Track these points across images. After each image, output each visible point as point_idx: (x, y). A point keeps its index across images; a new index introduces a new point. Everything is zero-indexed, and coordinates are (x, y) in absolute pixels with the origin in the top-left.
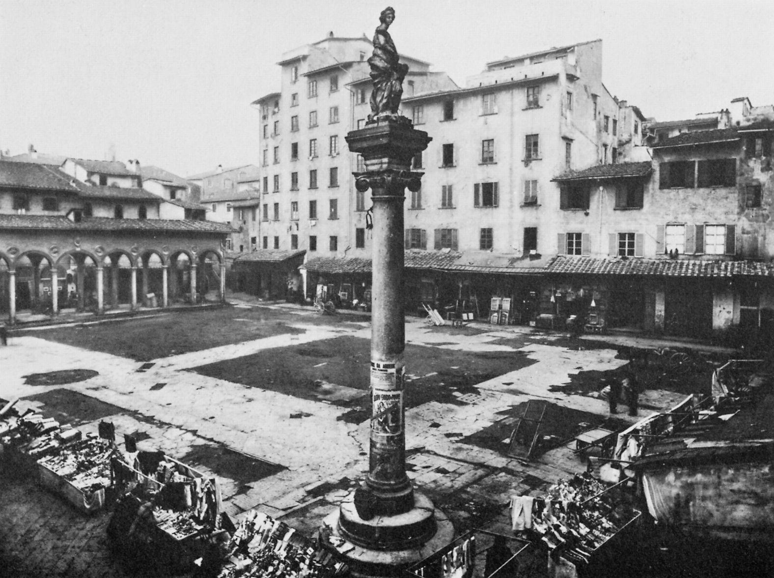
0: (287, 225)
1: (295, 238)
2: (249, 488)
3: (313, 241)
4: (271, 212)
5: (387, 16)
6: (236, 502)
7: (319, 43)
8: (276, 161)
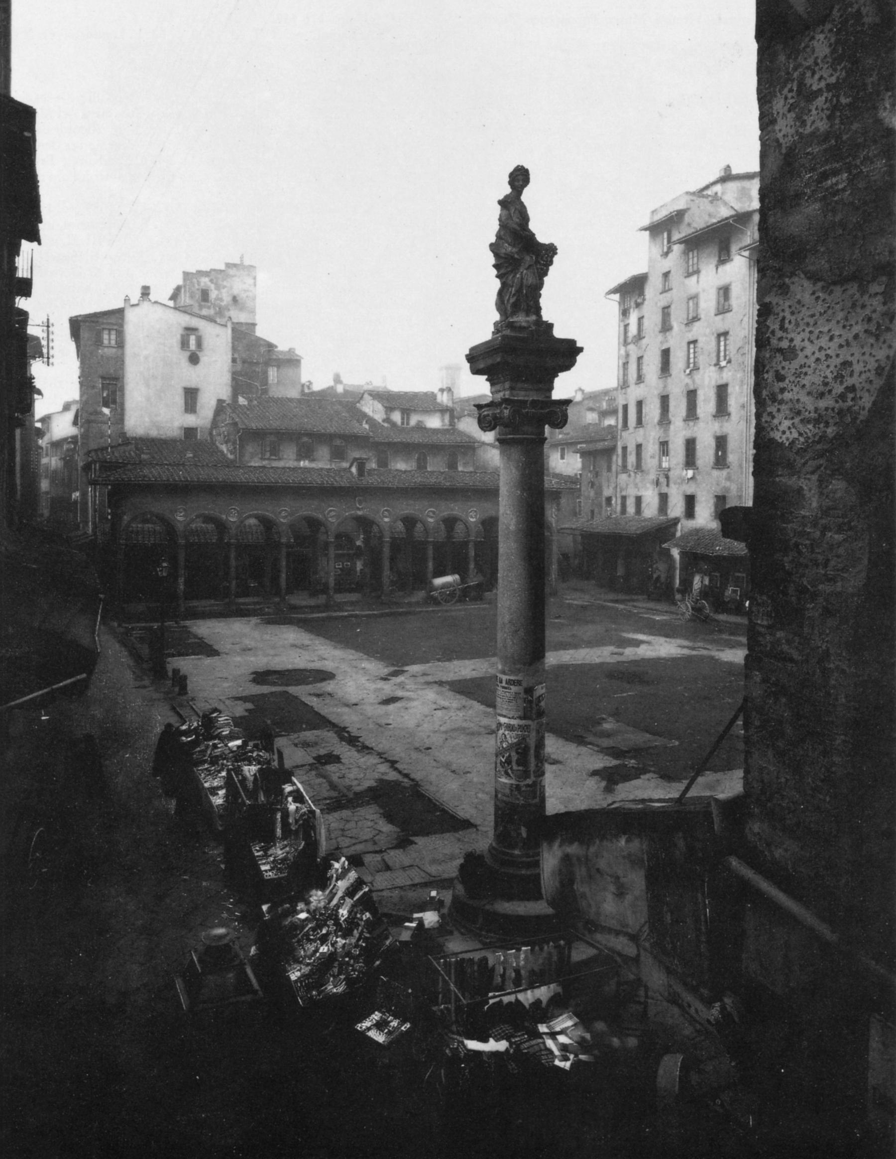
0: (652, 476)
1: (664, 498)
2: (412, 843)
3: (690, 501)
4: (632, 459)
5: (520, 178)
6: (386, 858)
7: (707, 187)
8: (640, 379)
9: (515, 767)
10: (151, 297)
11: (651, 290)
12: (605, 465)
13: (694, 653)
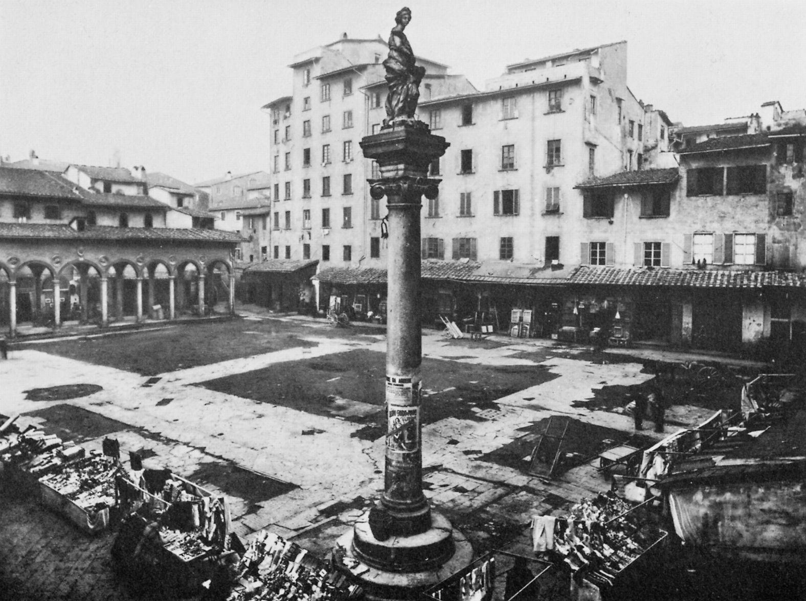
0: (299, 233)
1: (307, 248)
2: (260, 507)
3: (326, 250)
4: (282, 221)
5: (403, 17)
6: (246, 522)
7: (332, 45)
8: (287, 168)
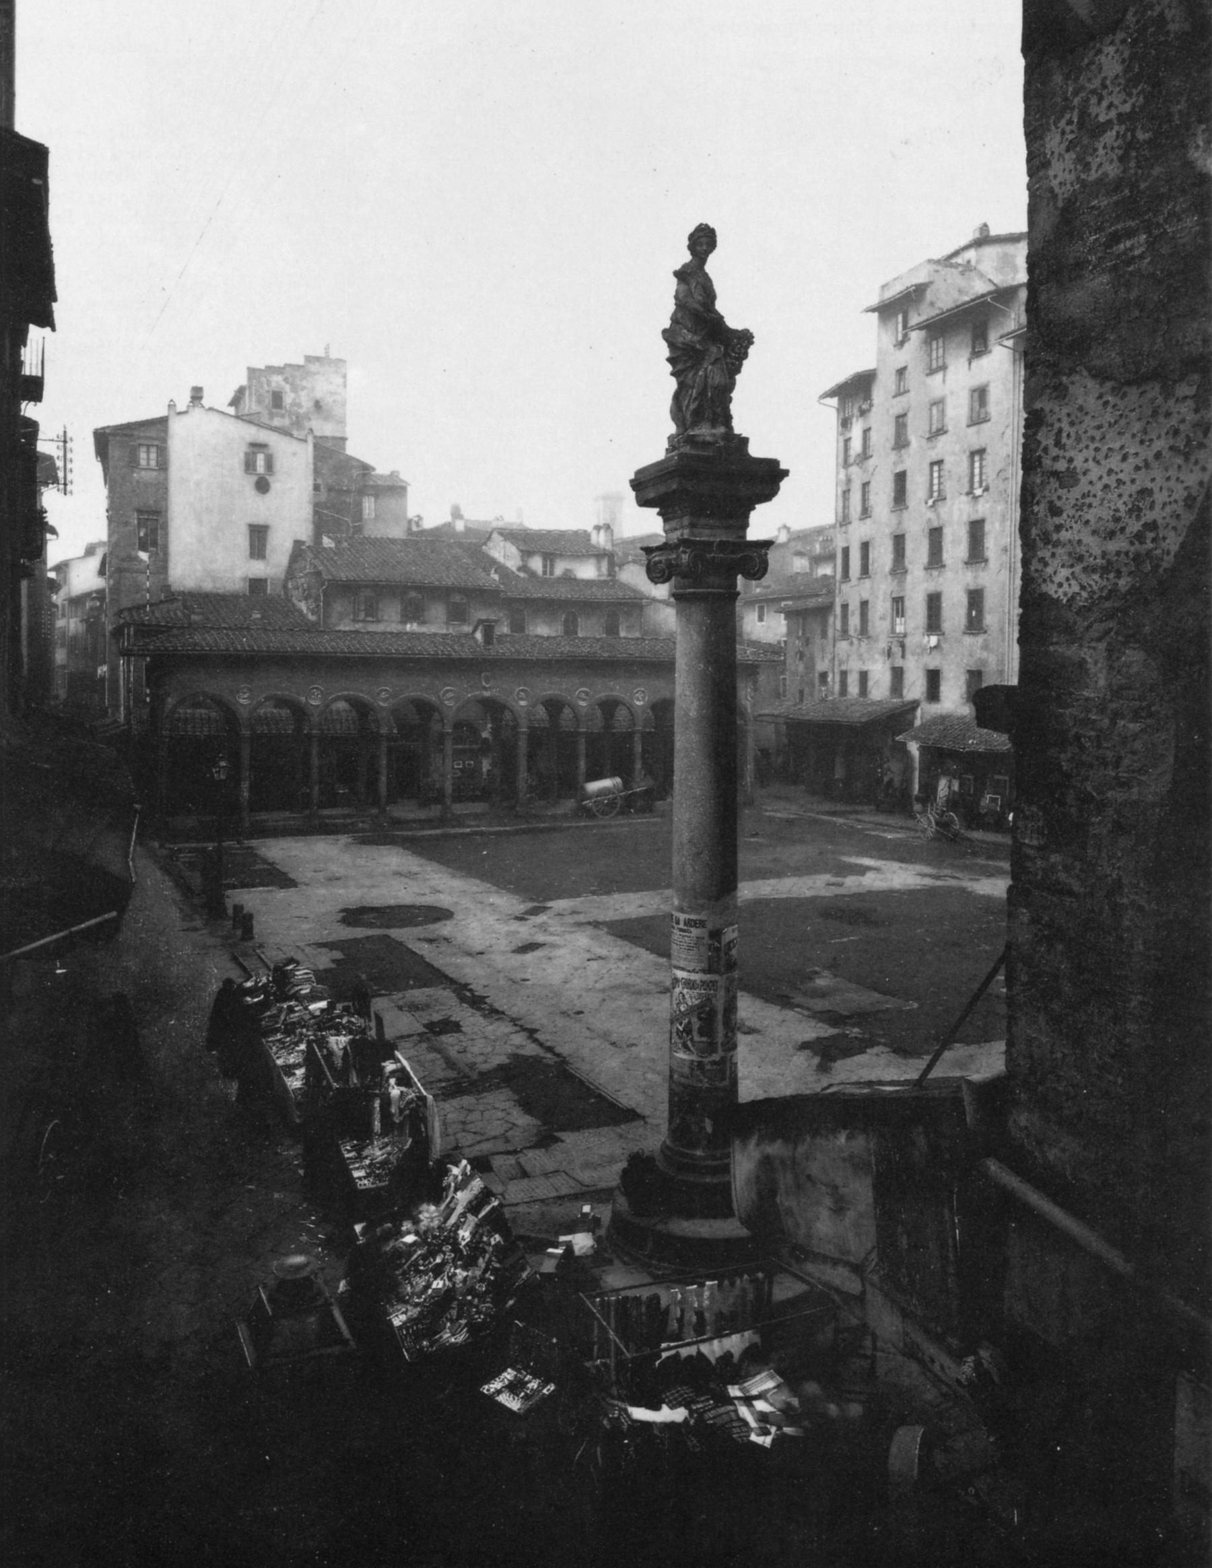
0: (882, 644)
1: (898, 674)
2: (558, 1140)
3: (934, 678)
4: (854, 621)
5: (703, 240)
6: (522, 1160)
7: (956, 253)
8: (866, 512)
9: (697, 1038)
10: (204, 402)
11: (881, 393)
12: (818, 630)
13: (939, 883)
